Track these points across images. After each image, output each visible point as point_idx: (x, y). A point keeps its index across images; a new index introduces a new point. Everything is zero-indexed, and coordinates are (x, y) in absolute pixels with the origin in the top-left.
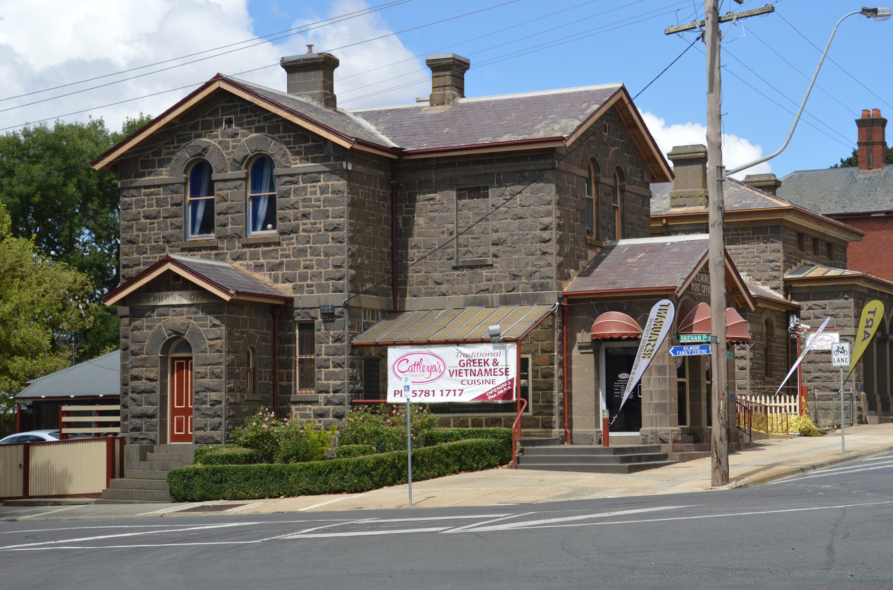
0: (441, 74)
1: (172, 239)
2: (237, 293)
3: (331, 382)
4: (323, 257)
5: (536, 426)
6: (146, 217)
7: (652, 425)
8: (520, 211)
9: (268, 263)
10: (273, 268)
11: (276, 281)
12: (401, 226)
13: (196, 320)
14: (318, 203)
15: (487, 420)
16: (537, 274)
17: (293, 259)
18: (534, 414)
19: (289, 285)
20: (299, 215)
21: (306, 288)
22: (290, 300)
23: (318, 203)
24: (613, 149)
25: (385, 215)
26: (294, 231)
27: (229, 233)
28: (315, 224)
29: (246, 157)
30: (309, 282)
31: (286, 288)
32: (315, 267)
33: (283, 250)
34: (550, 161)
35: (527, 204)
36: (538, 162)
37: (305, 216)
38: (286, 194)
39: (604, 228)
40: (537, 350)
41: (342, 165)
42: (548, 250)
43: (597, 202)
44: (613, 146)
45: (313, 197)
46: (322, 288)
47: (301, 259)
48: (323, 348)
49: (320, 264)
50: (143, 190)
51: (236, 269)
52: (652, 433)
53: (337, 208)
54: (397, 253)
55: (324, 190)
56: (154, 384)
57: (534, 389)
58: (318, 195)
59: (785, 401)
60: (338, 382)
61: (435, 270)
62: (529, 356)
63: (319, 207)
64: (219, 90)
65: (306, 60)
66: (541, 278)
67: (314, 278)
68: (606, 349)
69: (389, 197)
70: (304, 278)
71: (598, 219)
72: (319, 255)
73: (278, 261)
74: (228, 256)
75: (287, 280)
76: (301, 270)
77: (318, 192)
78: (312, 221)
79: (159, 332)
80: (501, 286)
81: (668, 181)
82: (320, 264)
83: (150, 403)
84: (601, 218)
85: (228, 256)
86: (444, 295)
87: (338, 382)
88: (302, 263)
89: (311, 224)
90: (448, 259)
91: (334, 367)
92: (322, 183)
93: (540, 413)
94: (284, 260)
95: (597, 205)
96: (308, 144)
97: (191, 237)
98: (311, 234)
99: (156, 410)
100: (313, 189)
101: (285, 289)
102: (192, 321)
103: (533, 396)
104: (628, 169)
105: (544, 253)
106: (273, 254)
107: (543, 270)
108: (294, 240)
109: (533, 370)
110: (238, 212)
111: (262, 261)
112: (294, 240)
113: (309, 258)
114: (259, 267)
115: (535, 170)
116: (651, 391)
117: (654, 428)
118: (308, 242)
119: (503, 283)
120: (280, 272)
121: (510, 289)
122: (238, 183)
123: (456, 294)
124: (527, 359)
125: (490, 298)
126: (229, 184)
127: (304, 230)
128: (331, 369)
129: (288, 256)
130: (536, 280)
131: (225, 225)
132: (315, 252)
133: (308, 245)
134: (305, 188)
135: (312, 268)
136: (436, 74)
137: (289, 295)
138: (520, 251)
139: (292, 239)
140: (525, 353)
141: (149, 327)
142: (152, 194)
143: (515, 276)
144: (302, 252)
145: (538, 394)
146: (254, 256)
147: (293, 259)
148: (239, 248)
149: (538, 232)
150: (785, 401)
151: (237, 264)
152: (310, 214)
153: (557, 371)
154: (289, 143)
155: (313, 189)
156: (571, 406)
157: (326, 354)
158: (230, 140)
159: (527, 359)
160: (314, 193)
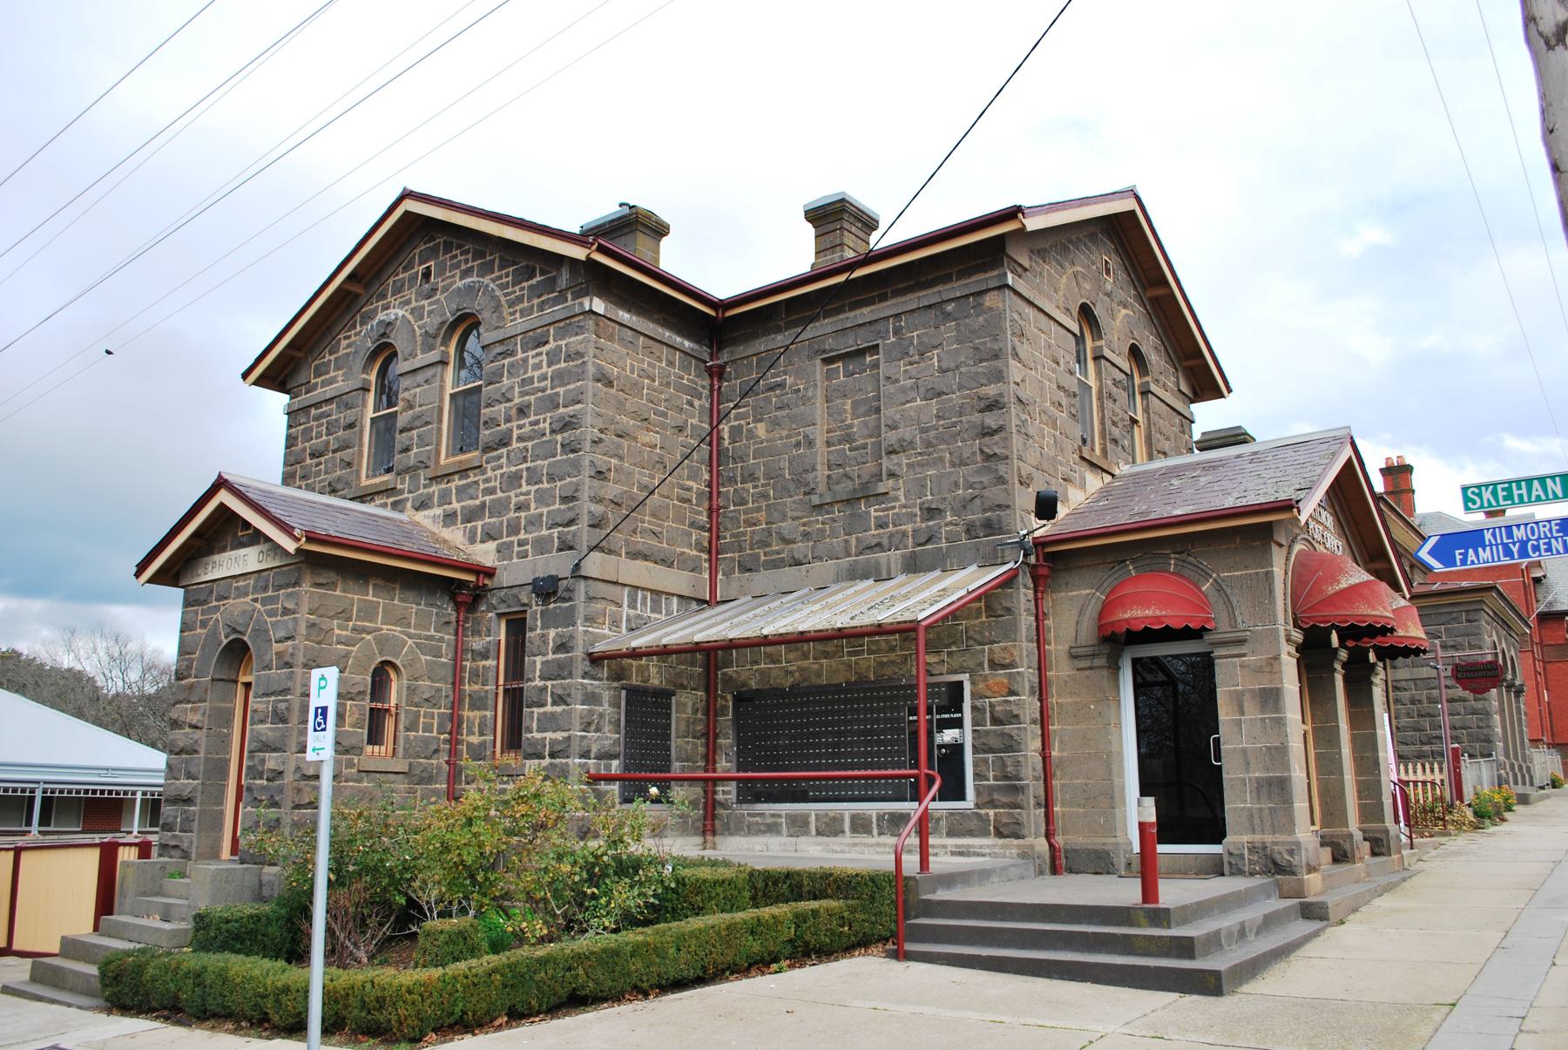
0: (831, 227)
1: (339, 486)
2: (311, 538)
3: (549, 735)
4: (545, 485)
5: (984, 833)
6: (313, 456)
7: (1253, 831)
8: (939, 382)
9: (463, 508)
10: (471, 515)
11: (472, 540)
12: (726, 443)
13: (264, 602)
14: (543, 384)
15: (880, 817)
16: (978, 502)
17: (500, 494)
18: (977, 806)
19: (492, 546)
20: (514, 412)
21: (516, 549)
22: (490, 573)
23: (543, 384)
24: (1124, 312)
25: (695, 421)
26: (504, 442)
27: (412, 461)
28: (537, 423)
29: (443, 323)
30: (522, 536)
31: (486, 552)
32: (533, 505)
33: (487, 481)
34: (995, 273)
35: (952, 365)
36: (973, 279)
37: (522, 411)
38: (494, 379)
39: (1115, 441)
40: (981, 664)
41: (581, 304)
42: (998, 451)
43: (1100, 392)
44: (1125, 307)
45: (536, 374)
46: (542, 546)
47: (512, 494)
48: (539, 666)
49: (541, 498)
50: (313, 411)
51: (417, 524)
52: (1253, 849)
53: (572, 386)
54: (719, 493)
55: (553, 358)
56: (198, 734)
57: (976, 750)
58: (545, 369)
59: (1432, 770)
60: (559, 735)
61: (784, 518)
62: (965, 677)
63: (543, 390)
64: (407, 214)
65: (1123, 788)
66: (984, 511)
67: (529, 528)
68: (1135, 662)
69: (706, 392)
70: (514, 529)
71: (1102, 423)
72: (541, 482)
73: (477, 502)
74: (409, 504)
75: (489, 536)
76: (512, 515)
77: (544, 364)
78: (533, 418)
79: (214, 634)
80: (904, 534)
81: (1222, 396)
82: (541, 498)
83: (190, 776)
84: (1108, 423)
85: (409, 504)
86: (798, 563)
87: (559, 735)
88: (514, 500)
89: (531, 424)
90: (806, 494)
91: (554, 703)
92: (552, 345)
93: (992, 804)
94: (487, 498)
95: (1100, 399)
96: (533, 282)
97: (364, 482)
98: (530, 444)
99: (194, 789)
100: (537, 360)
101: (485, 553)
102: (258, 605)
103: (975, 765)
104: (1154, 358)
105: (988, 457)
106: (472, 491)
107: (986, 493)
108: (504, 460)
109: (974, 708)
110: (427, 423)
111: (456, 505)
112: (504, 460)
113: (525, 488)
114: (449, 518)
115: (967, 296)
116: (1244, 751)
117: (1258, 838)
118: (525, 460)
119: (909, 528)
120: (480, 523)
121: (923, 540)
122: (430, 372)
123: (821, 559)
124: (961, 683)
125: (883, 562)
126: (420, 377)
127: (520, 439)
128: (549, 708)
129: (491, 491)
130: (976, 517)
131: (407, 450)
132: (534, 477)
133: (524, 466)
134: (525, 360)
135: (528, 508)
136: (823, 229)
137: (489, 564)
138: (941, 459)
139: (500, 457)
140: (956, 672)
141: (204, 624)
142: (323, 415)
143: (931, 512)
144: (513, 480)
145: (986, 761)
146: (445, 499)
147: (500, 494)
148: (425, 486)
149: (976, 417)
150: (1432, 770)
151: (420, 517)
152: (529, 406)
153: (1029, 706)
154: (506, 286)
155: (537, 360)
156: (761, 963)
157: (542, 678)
158: (425, 302)
159: (961, 683)
160: (538, 366)
